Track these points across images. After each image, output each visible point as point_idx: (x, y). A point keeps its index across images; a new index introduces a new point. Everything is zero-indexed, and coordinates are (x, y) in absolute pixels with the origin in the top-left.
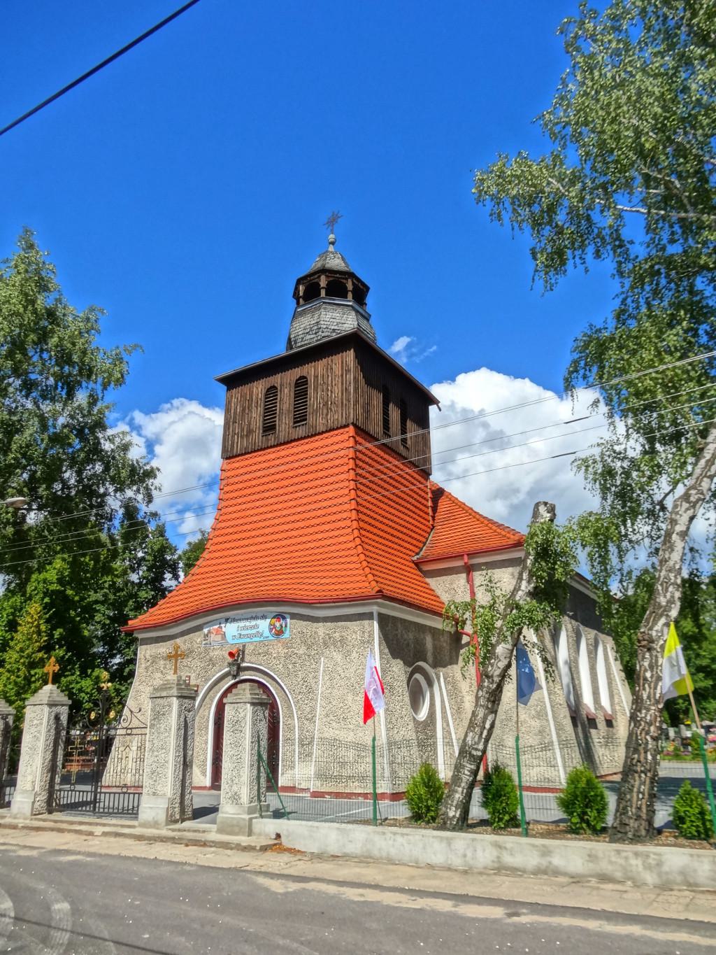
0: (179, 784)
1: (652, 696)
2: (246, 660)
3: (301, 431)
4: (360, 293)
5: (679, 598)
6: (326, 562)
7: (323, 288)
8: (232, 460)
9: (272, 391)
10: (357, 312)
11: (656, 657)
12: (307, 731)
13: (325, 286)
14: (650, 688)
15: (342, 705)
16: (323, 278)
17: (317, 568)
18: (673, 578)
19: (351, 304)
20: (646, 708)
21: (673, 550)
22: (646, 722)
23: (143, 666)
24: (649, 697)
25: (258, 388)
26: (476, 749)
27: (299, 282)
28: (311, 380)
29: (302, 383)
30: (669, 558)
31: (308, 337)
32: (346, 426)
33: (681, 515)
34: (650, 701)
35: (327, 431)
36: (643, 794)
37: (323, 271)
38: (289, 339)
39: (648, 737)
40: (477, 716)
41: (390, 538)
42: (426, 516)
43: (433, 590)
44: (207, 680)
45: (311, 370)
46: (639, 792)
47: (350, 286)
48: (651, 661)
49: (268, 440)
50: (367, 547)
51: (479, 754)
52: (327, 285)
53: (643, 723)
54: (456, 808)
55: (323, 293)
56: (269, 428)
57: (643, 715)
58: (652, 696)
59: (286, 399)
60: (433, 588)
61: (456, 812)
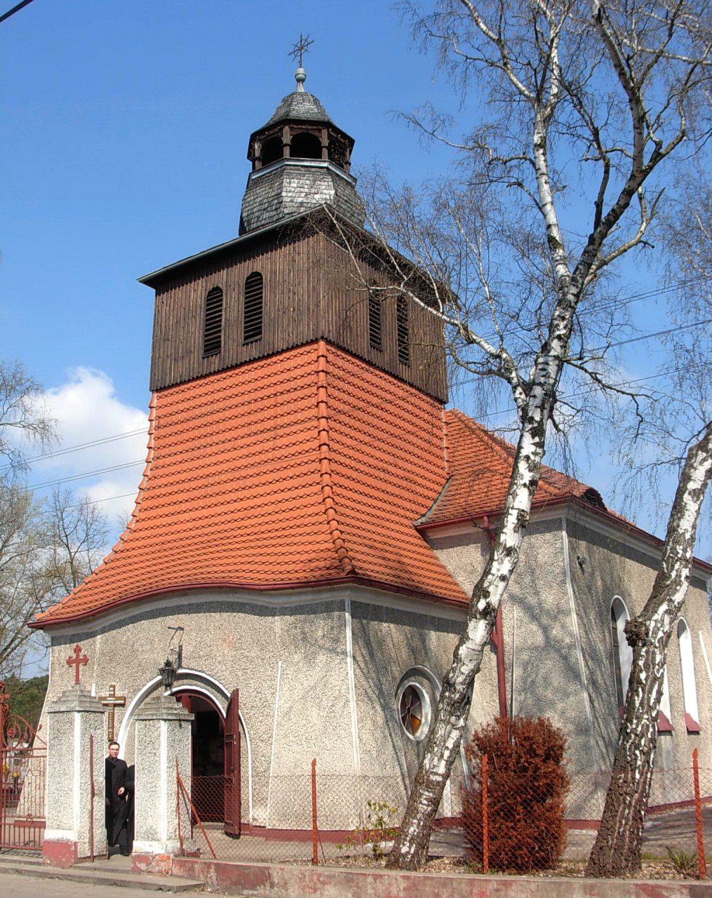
0: (87, 816)
1: (645, 702)
2: (183, 664)
3: (254, 351)
4: (341, 146)
5: (687, 577)
6: (286, 533)
7: (286, 145)
8: (165, 393)
9: (215, 296)
10: (336, 178)
11: (654, 653)
12: (263, 756)
13: (289, 142)
14: (644, 693)
15: (304, 722)
16: (287, 129)
17: (273, 542)
18: (681, 552)
19: (326, 165)
20: (637, 718)
21: (682, 516)
22: (636, 735)
23: (57, 672)
24: (641, 704)
25: (196, 291)
26: (436, 774)
27: (254, 138)
28: (266, 277)
29: (254, 282)
30: (678, 526)
31: (266, 215)
32: (315, 341)
33: (695, 469)
34: (643, 709)
35: (288, 350)
36: (627, 820)
37: (285, 121)
38: (242, 218)
39: (637, 752)
40: (437, 733)
41: (381, 495)
42: (439, 462)
43: (442, 567)
44: (135, 692)
45: (260, 264)
46: (622, 817)
47: (325, 141)
48: (647, 659)
49: (210, 364)
50: (343, 510)
51: (440, 779)
52: (292, 141)
53: (633, 736)
54: (410, 841)
55: (287, 151)
56: (212, 346)
57: (634, 726)
58: (645, 702)
59: (233, 306)
60: (443, 563)
61: (410, 848)
